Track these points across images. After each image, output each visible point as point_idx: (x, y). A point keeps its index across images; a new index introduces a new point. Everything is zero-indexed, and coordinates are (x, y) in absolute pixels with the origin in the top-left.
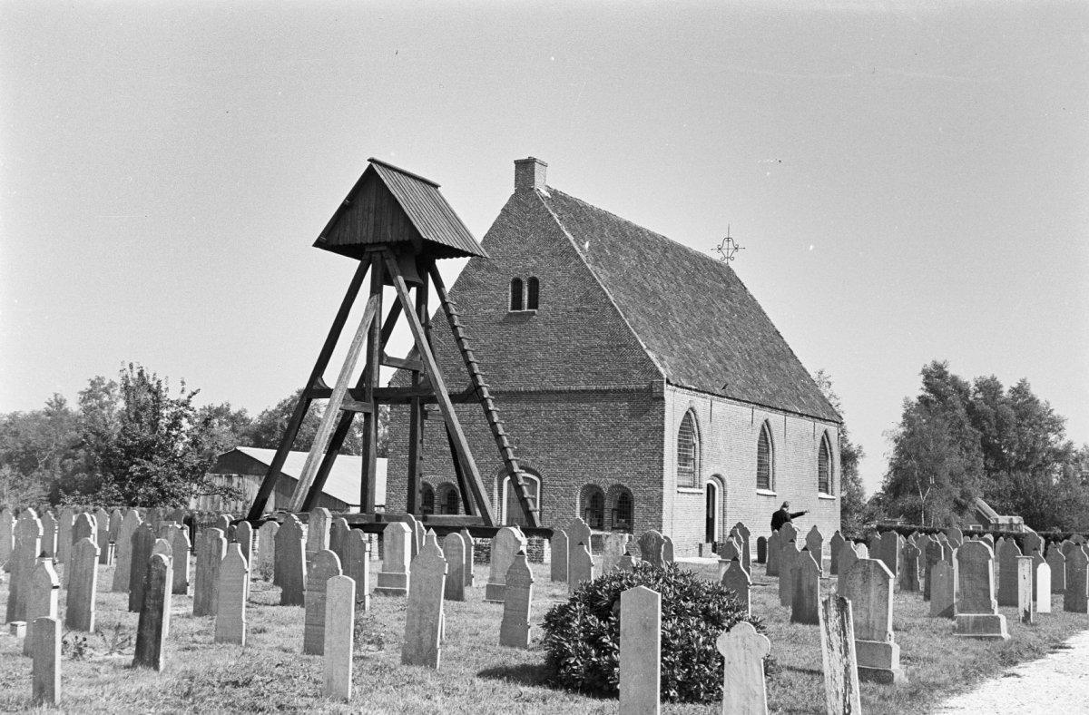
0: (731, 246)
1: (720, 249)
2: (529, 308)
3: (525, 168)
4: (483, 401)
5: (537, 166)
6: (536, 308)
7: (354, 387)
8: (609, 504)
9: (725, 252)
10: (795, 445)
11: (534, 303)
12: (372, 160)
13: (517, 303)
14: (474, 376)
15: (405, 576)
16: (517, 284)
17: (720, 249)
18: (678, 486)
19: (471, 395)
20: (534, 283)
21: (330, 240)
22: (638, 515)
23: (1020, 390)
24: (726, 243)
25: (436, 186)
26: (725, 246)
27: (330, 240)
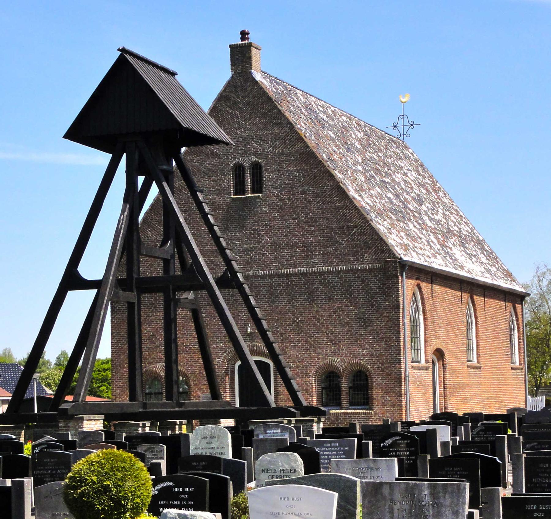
0: (406, 123)
1: (395, 127)
2: (253, 192)
3: (241, 55)
4: (240, 286)
5: (254, 51)
6: (261, 192)
7: (69, 292)
8: (345, 384)
9: (401, 129)
10: (492, 317)
11: (257, 187)
12: (123, 50)
13: (240, 188)
14: (228, 262)
15: (177, 472)
16: (239, 170)
17: (395, 127)
18: (412, 362)
19: (228, 281)
20: (257, 169)
21: (80, 132)
22: (377, 392)
23: (508, 410)
24: (401, 120)
25: (173, 74)
26: (401, 123)
27: (80, 132)
